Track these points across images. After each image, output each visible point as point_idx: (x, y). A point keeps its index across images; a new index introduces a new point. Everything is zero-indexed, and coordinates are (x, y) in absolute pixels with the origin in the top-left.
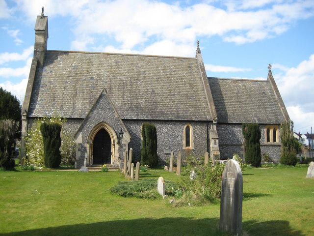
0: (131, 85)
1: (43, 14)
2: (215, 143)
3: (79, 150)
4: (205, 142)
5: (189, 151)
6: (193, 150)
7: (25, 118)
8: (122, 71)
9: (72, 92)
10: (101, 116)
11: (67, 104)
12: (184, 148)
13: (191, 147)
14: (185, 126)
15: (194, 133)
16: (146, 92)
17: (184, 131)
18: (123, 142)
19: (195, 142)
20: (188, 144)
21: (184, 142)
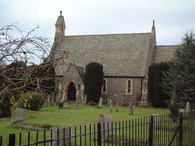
1: (61, 15)
2: (145, 91)
5: (129, 95)
12: (127, 93)
13: (131, 94)
14: (128, 80)
17: (127, 83)
18: (81, 90)
20: (129, 91)
21: (127, 90)
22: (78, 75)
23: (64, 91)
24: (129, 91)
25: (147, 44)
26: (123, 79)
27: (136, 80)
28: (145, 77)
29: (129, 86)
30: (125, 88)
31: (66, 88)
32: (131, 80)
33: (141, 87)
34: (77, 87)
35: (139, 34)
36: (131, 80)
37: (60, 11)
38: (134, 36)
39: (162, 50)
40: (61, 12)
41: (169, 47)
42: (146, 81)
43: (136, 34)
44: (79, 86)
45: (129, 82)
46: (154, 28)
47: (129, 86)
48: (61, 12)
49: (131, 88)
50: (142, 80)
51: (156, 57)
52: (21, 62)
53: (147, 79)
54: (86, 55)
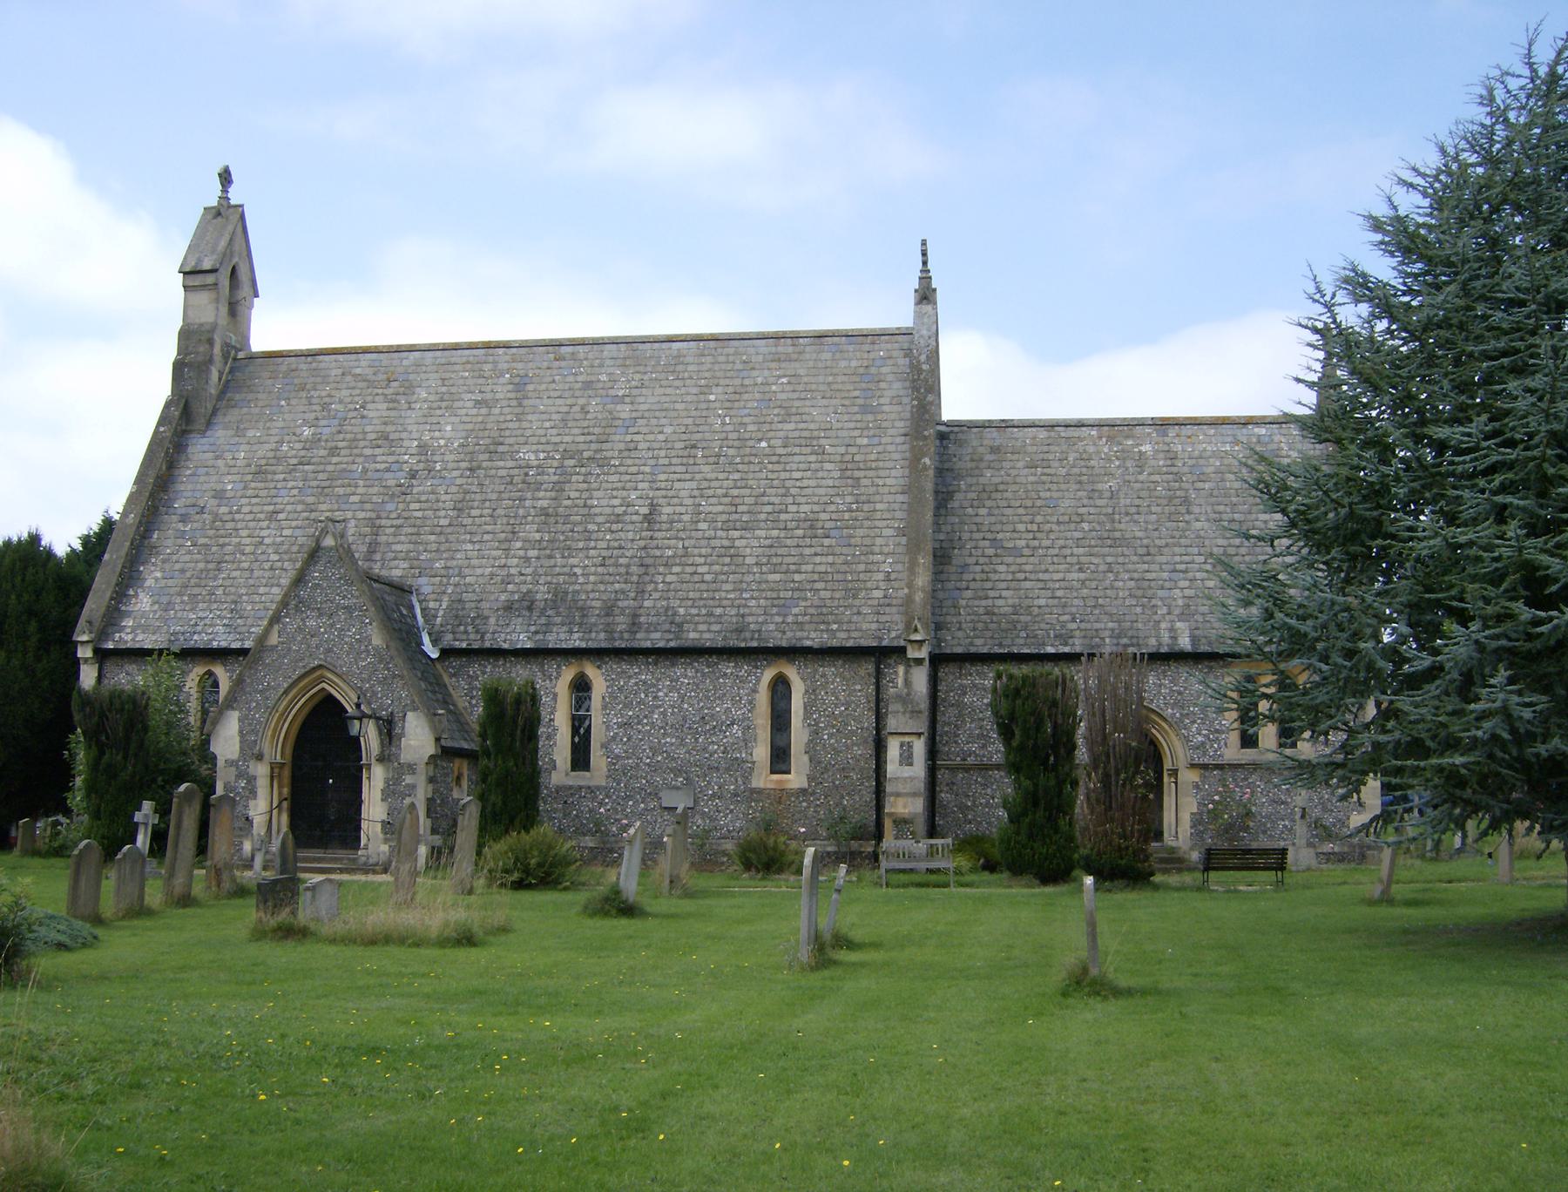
0: (559, 487)
1: (224, 198)
2: (907, 759)
3: (1327, 742)
4: (864, 751)
5: (781, 795)
6: (803, 791)
7: (89, 654)
8: (534, 422)
9: (298, 532)
10: (314, 642)
11: (262, 590)
12: (764, 780)
13: (796, 779)
14: (768, 675)
15: (807, 708)
16: (618, 519)
17: (763, 698)
18: (406, 757)
19: (810, 749)
20: (780, 758)
21: (761, 752)
22: (377, 640)
23: (261, 771)
24: (780, 758)
25: (886, 408)
26: (728, 668)
27: (830, 671)
28: (901, 651)
29: (780, 721)
30: (747, 741)
31: (275, 748)
32: (792, 673)
33: (878, 729)
34: (370, 738)
35: (820, 336)
36: (792, 673)
37: (218, 169)
38: (785, 348)
39: (995, 450)
40: (226, 178)
41: (1042, 434)
42: (907, 683)
43: (795, 337)
44: (389, 730)
45: (780, 688)
46: (926, 295)
47: (780, 721)
48: (226, 178)
49: (799, 734)
50: (879, 675)
51: (956, 504)
52: (1105, 879)
53: (919, 661)
54: (422, 487)
